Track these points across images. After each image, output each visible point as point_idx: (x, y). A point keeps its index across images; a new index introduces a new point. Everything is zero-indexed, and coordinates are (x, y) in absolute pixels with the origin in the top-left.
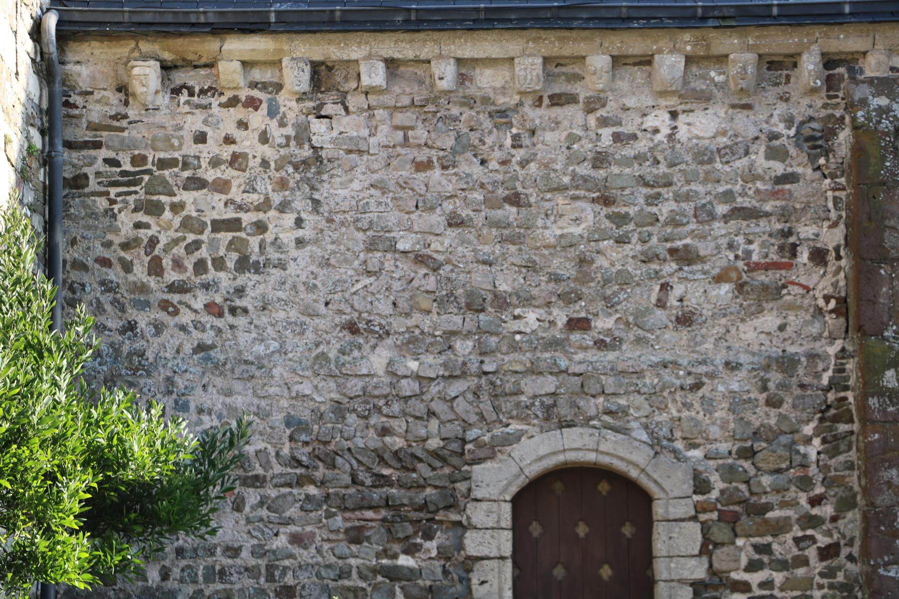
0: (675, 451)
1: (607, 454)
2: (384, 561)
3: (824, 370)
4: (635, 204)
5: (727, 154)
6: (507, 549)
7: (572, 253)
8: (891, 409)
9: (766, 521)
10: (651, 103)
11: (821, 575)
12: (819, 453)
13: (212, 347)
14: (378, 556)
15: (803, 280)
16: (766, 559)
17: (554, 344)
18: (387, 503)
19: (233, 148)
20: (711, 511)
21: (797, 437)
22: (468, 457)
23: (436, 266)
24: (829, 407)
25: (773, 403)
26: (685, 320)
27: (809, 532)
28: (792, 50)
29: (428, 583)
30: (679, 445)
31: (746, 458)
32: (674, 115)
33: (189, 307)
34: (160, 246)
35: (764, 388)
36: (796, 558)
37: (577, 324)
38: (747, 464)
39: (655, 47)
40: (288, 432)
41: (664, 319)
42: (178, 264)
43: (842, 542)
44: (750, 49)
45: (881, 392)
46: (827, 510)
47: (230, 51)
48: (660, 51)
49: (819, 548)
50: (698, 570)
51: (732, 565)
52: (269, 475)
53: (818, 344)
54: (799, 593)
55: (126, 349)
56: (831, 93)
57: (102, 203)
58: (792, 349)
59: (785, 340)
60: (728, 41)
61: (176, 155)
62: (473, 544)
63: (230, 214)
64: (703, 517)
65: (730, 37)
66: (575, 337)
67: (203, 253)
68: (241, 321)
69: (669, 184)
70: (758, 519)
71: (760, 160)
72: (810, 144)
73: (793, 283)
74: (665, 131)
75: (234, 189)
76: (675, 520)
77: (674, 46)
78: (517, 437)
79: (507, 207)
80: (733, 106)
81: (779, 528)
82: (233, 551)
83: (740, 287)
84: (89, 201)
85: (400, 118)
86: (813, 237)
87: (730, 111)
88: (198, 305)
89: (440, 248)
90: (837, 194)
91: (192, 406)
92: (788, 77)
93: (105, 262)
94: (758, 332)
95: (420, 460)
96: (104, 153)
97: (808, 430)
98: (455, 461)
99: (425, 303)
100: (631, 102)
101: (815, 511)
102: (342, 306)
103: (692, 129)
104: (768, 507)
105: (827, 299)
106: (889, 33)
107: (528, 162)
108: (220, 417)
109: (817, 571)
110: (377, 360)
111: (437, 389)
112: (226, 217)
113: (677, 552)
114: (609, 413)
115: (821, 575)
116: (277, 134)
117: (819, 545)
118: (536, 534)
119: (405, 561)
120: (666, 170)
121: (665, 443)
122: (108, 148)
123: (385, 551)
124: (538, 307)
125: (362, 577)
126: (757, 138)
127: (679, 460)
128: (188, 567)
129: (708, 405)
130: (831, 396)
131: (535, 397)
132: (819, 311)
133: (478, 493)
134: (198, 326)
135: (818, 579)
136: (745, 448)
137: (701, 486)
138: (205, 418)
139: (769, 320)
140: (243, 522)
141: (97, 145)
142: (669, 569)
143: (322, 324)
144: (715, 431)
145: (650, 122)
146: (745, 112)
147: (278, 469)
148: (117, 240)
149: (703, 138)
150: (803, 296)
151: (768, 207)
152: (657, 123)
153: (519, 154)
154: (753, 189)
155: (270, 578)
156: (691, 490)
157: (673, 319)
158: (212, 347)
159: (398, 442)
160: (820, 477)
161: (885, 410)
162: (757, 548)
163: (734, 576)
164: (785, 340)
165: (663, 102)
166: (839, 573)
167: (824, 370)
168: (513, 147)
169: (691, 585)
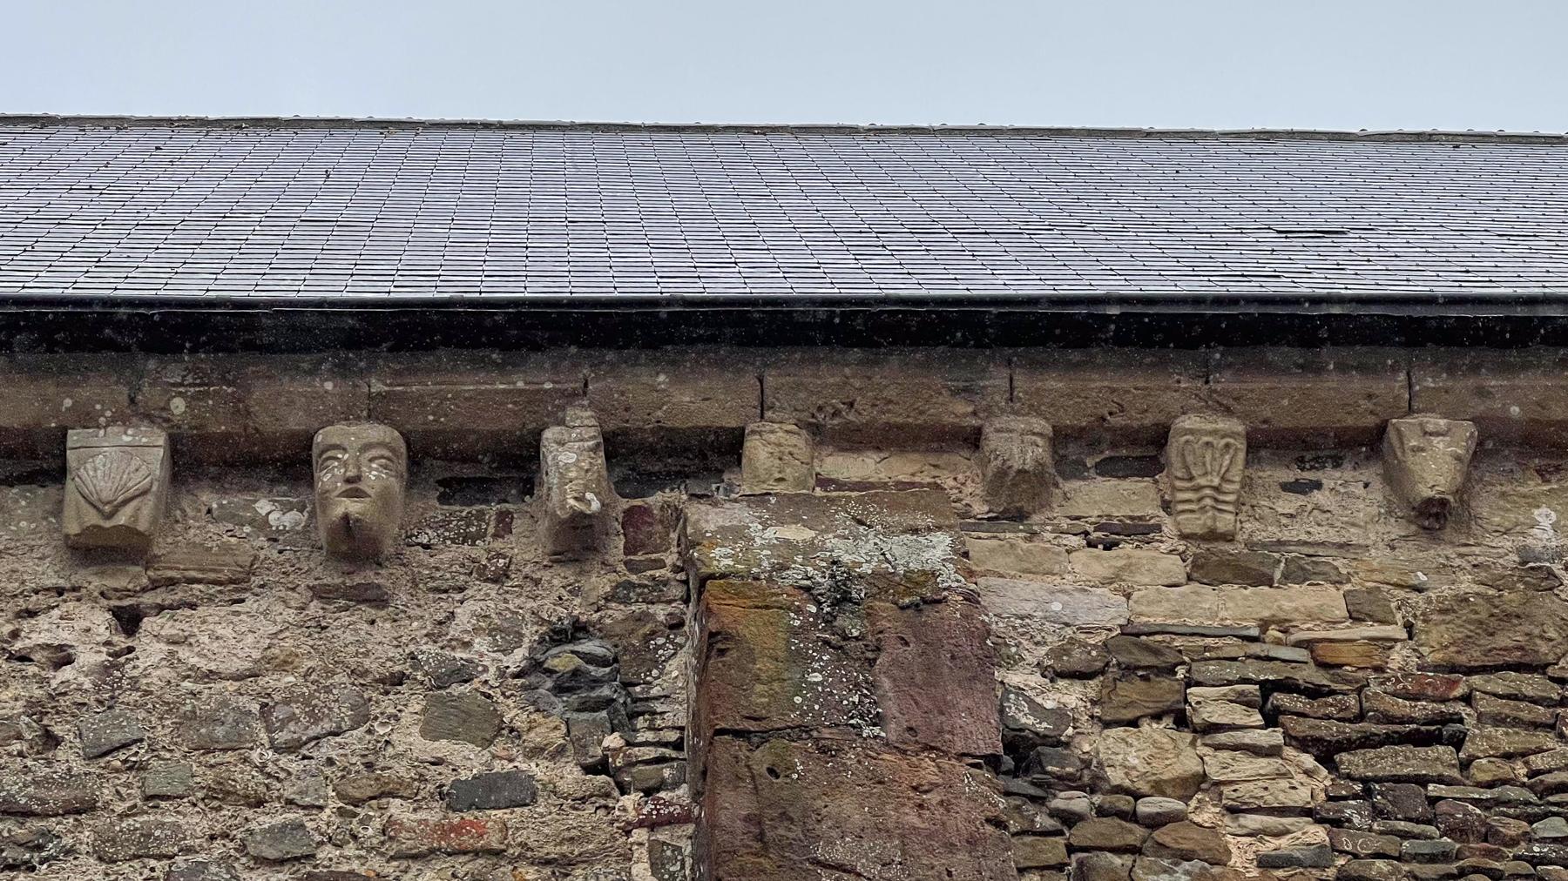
5: (292, 718)
10: (50, 581)
28: (506, 421)
32: (129, 621)
39: (68, 402)
44: (377, 411)
48: (87, 419)
56: (639, 557)
60: (298, 387)
65: (313, 372)
69: (82, 808)
71: (408, 738)
72: (573, 698)
74: (89, 657)
77: (132, 401)
80: (322, 594)
87: (315, 608)
90: (663, 835)
103: (183, 652)
106: (807, 376)
120: (78, 766)
126: (398, 680)
146: (369, 612)
149: (211, 676)
152: (64, 636)
154: (377, 824)
165: (94, 582)
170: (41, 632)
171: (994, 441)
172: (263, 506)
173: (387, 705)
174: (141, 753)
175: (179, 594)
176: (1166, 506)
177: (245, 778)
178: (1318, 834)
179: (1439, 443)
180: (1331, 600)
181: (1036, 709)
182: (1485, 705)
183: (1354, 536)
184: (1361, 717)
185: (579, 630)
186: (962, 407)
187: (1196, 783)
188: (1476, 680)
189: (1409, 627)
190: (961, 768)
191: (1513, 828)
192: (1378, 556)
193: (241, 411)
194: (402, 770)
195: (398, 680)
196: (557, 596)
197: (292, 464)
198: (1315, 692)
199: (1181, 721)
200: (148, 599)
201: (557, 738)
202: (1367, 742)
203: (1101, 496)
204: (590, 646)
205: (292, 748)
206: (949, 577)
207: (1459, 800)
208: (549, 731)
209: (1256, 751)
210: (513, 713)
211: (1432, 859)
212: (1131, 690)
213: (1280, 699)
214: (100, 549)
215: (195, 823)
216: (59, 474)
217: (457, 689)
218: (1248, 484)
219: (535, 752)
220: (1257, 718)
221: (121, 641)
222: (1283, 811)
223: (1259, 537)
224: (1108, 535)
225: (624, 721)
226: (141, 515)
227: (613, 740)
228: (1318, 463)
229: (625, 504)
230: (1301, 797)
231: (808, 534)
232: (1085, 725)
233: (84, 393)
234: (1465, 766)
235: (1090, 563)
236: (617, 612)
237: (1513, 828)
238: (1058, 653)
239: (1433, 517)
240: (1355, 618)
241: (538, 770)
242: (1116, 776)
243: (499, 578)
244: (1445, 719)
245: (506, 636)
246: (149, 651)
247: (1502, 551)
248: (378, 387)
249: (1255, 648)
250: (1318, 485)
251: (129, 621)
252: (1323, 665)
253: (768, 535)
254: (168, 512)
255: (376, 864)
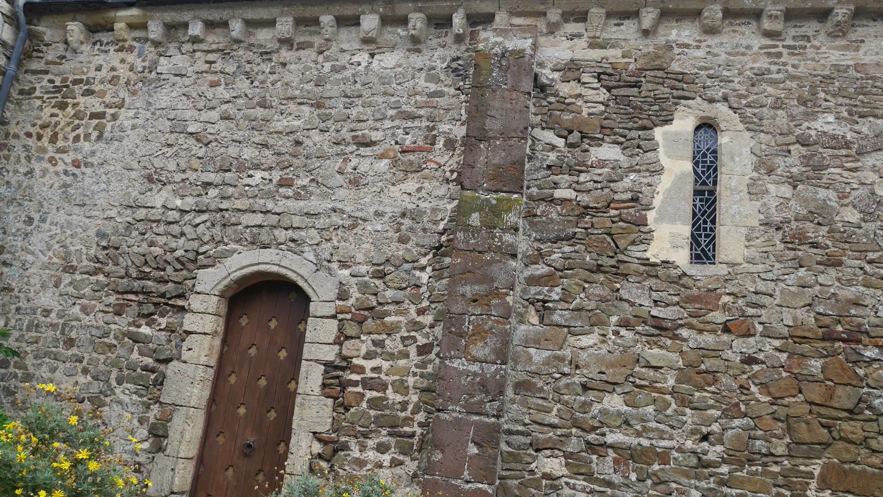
0: (329, 269)
1: (286, 268)
2: (132, 329)
3: (442, 220)
4: (338, 107)
6: (306, 347)
7: (292, 137)
8: (472, 241)
9: (383, 324)
10: (358, 47)
11: (417, 366)
12: (430, 277)
13: (70, 186)
14: (129, 324)
15: (438, 159)
16: (379, 350)
17: (270, 195)
18: (144, 292)
19: (115, 73)
20: (346, 313)
21: (416, 264)
22: (199, 263)
23: (206, 142)
24: (441, 246)
25: (403, 240)
26: (355, 183)
27: (413, 334)
29: (155, 346)
30: (335, 266)
31: (378, 278)
32: (372, 55)
33: (63, 161)
34: (60, 127)
35: (398, 230)
36: (400, 352)
37: (285, 183)
38: (378, 282)
40: (96, 239)
41: (341, 181)
42: (66, 138)
43: (435, 343)
44: (420, 10)
45: (467, 228)
46: (428, 319)
47: (120, 16)
48: (364, 13)
49: (418, 346)
50: (330, 354)
51: (355, 353)
52: (79, 266)
53: (441, 203)
54: (398, 378)
55: (25, 184)
57: (38, 103)
58: (423, 205)
59: (419, 199)
61: (84, 77)
62: (189, 322)
63: (101, 109)
64: (340, 316)
66: (282, 190)
67: (80, 131)
68: (89, 171)
69: (360, 96)
70: (378, 322)
71: (421, 82)
73: (431, 161)
74: (364, 64)
75: (107, 96)
76: (322, 317)
78: (234, 251)
79: (258, 108)
80: (409, 50)
81: (391, 331)
82: (47, 312)
83: (395, 162)
84: (32, 101)
85: (211, 57)
86: (448, 131)
88: (68, 160)
89: (212, 132)
91: (49, 220)
92: (447, 32)
93: (29, 135)
94: (401, 195)
95: (169, 263)
96: (50, 76)
97: (424, 261)
98: (191, 266)
99: (196, 163)
100: (345, 46)
101: (420, 319)
102: (147, 164)
104: (387, 314)
105: (452, 172)
107: (277, 82)
108: (62, 227)
109: (414, 362)
110: (158, 198)
111: (189, 218)
112: (98, 110)
113: (317, 340)
114: (293, 241)
115: (417, 366)
116: (139, 66)
117: (418, 343)
118: (244, 324)
119: (145, 330)
120: (360, 88)
121: (325, 263)
122: (52, 73)
123: (134, 322)
124: (263, 170)
125: (116, 338)
126: (422, 69)
127: (331, 275)
128: (20, 319)
129: (359, 240)
130: (444, 238)
131: (247, 227)
132: (448, 181)
133: (198, 288)
134: (66, 173)
135: (413, 369)
136: (378, 271)
137: (343, 295)
138: (54, 228)
139: (411, 185)
140: (57, 294)
141: (46, 72)
142: (310, 352)
143: (134, 175)
144: (360, 257)
145: (356, 59)
146: (417, 54)
147: (85, 263)
148: (39, 122)
149: (386, 68)
150: (436, 170)
151: (422, 112)
152: (360, 60)
153: (272, 78)
155: (62, 333)
156: (336, 296)
157: (347, 181)
158: (70, 186)
159: (157, 251)
160: (427, 295)
161: (468, 242)
162: (374, 343)
163: (355, 361)
164: (419, 199)
165: (366, 47)
166: (429, 366)
167: (442, 220)
168: (270, 73)
169: (325, 365)
170: (356, 59)
171: (548, 15)
172: (399, 30)
173: (418, 75)
174: (371, 85)
175: (382, 50)
176: (586, 30)
177: (391, 91)
178: (602, 108)
179: (650, 15)
180: (618, 52)
181: (547, 78)
182: (648, 78)
183: (628, 37)
184: (619, 81)
185: (458, 58)
186: (542, 7)
187: (580, 95)
188: (648, 72)
189: (636, 60)
190: (521, 95)
191: (646, 107)
192: (632, 42)
193: (393, 10)
194: (420, 89)
195: (422, 69)
196: (454, 51)
197: (404, 21)
198: (610, 75)
199: (579, 81)
200: (376, 51)
201: (450, 83)
202: (619, 87)
203: (572, 27)
204: (460, 62)
205: (399, 84)
206: (529, 51)
207: (637, 101)
208: (449, 81)
209: (594, 89)
210: (442, 77)
211: (627, 114)
212: (569, 74)
213: (602, 76)
214: (366, 41)
215: (380, 99)
216: (358, 24)
217: (432, 72)
218: (605, 24)
219: (446, 86)
220: (596, 81)
221: (370, 60)
222: (597, 102)
223: (606, 37)
224: (572, 37)
225: (464, 80)
226: (373, 34)
227: (461, 83)
228: (624, 19)
229: (471, 29)
230: (601, 99)
231: (131, 328)
232: (558, 81)
233: (364, 7)
234: (640, 93)
235: (567, 44)
236: (466, 54)
237: (646, 107)
238: (554, 65)
239: (646, 33)
240: (623, 57)
241: (446, 89)
242: (561, 94)
243: (444, 46)
244: (637, 82)
245: (443, 60)
246: (375, 63)
247: (661, 40)
248: (420, 5)
249: (599, 64)
250: (622, 24)
251: (372, 55)
252: (613, 68)
253: (494, 39)
254: (380, 32)
255: (413, 109)
